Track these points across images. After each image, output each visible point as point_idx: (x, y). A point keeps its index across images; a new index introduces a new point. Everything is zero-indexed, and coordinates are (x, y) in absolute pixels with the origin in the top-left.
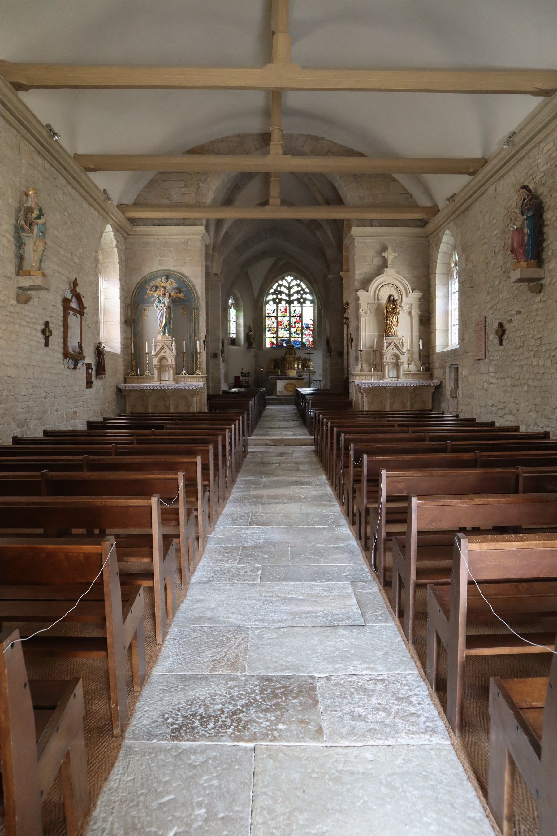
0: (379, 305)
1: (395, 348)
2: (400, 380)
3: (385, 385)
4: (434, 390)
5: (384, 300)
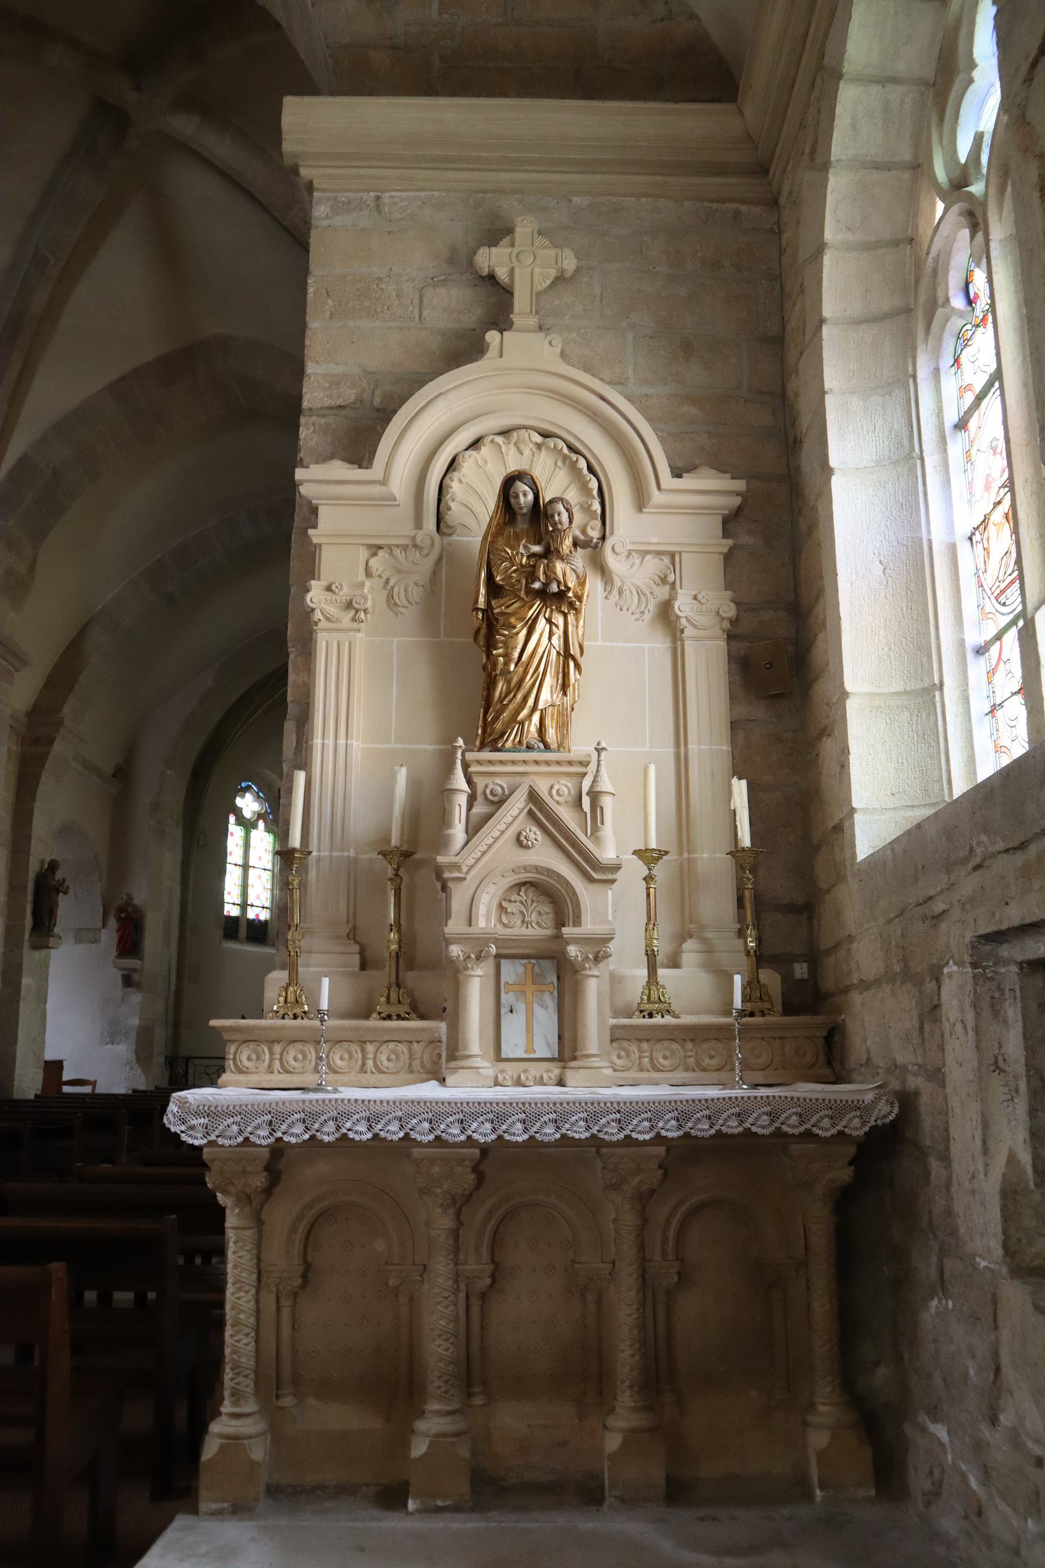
0: (447, 560)
1: (534, 834)
2: (582, 1088)
3: (393, 1132)
4: (844, 1174)
5: (475, 500)
